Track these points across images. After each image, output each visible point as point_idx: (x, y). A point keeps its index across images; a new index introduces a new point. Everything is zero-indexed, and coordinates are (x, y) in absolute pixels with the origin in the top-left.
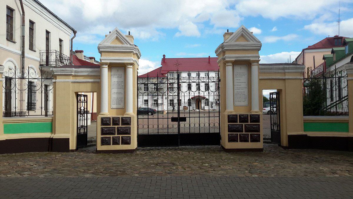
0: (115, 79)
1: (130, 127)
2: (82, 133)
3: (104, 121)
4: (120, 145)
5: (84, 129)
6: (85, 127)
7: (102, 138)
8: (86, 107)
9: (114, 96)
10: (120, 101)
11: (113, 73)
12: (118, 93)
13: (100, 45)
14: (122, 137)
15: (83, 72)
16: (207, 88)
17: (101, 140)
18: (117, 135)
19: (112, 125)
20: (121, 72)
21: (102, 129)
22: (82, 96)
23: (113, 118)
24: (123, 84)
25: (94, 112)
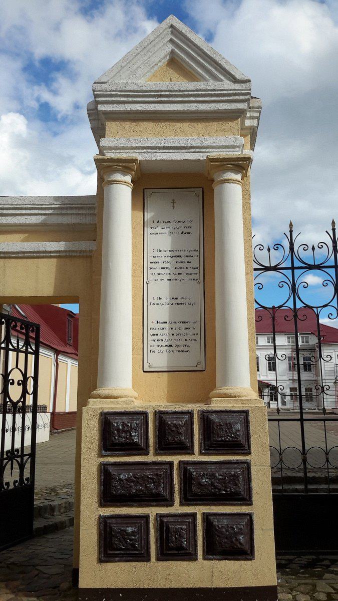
0: (161, 241)
1: (248, 465)
2: (12, 486)
3: (117, 432)
4: (196, 559)
5: (22, 467)
6: (25, 458)
7: (105, 524)
8: (31, 373)
9: (159, 313)
10: (184, 338)
11: (151, 214)
12: (175, 301)
13: (99, 87)
14: (206, 516)
15: (24, 212)
16: (272, 367)
17: (100, 535)
18: (182, 504)
19: (156, 454)
20: (188, 211)
21: (105, 473)
22: (19, 324)
23: (160, 416)
24: (195, 262)
25: (57, 410)
